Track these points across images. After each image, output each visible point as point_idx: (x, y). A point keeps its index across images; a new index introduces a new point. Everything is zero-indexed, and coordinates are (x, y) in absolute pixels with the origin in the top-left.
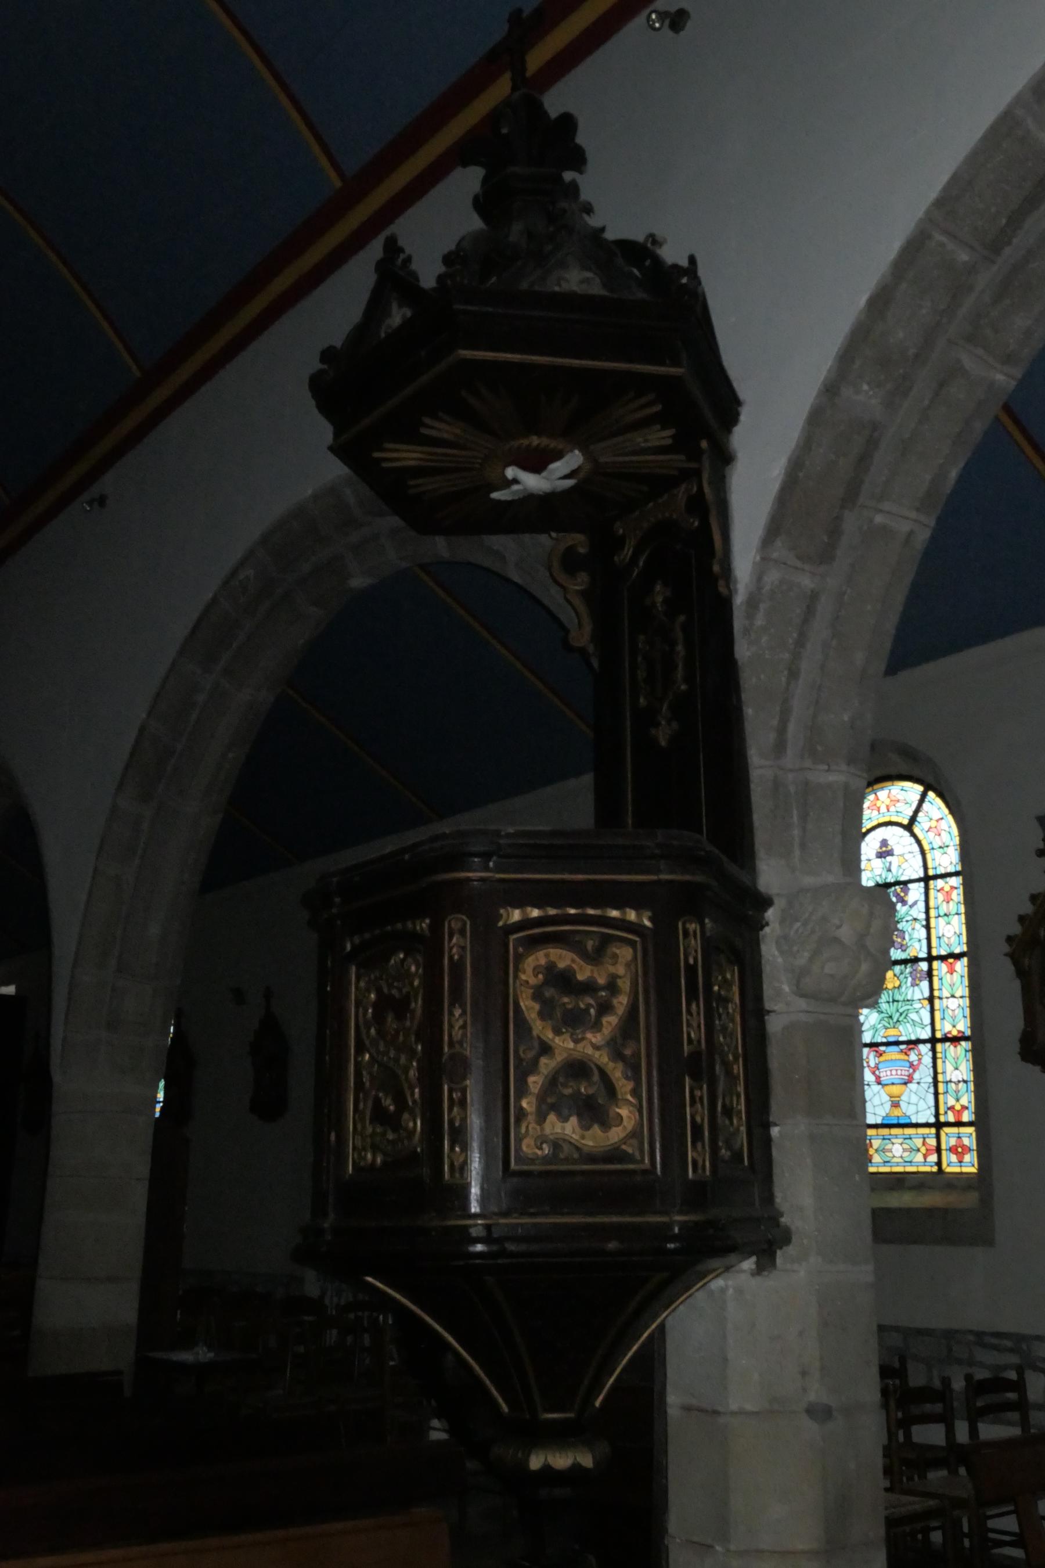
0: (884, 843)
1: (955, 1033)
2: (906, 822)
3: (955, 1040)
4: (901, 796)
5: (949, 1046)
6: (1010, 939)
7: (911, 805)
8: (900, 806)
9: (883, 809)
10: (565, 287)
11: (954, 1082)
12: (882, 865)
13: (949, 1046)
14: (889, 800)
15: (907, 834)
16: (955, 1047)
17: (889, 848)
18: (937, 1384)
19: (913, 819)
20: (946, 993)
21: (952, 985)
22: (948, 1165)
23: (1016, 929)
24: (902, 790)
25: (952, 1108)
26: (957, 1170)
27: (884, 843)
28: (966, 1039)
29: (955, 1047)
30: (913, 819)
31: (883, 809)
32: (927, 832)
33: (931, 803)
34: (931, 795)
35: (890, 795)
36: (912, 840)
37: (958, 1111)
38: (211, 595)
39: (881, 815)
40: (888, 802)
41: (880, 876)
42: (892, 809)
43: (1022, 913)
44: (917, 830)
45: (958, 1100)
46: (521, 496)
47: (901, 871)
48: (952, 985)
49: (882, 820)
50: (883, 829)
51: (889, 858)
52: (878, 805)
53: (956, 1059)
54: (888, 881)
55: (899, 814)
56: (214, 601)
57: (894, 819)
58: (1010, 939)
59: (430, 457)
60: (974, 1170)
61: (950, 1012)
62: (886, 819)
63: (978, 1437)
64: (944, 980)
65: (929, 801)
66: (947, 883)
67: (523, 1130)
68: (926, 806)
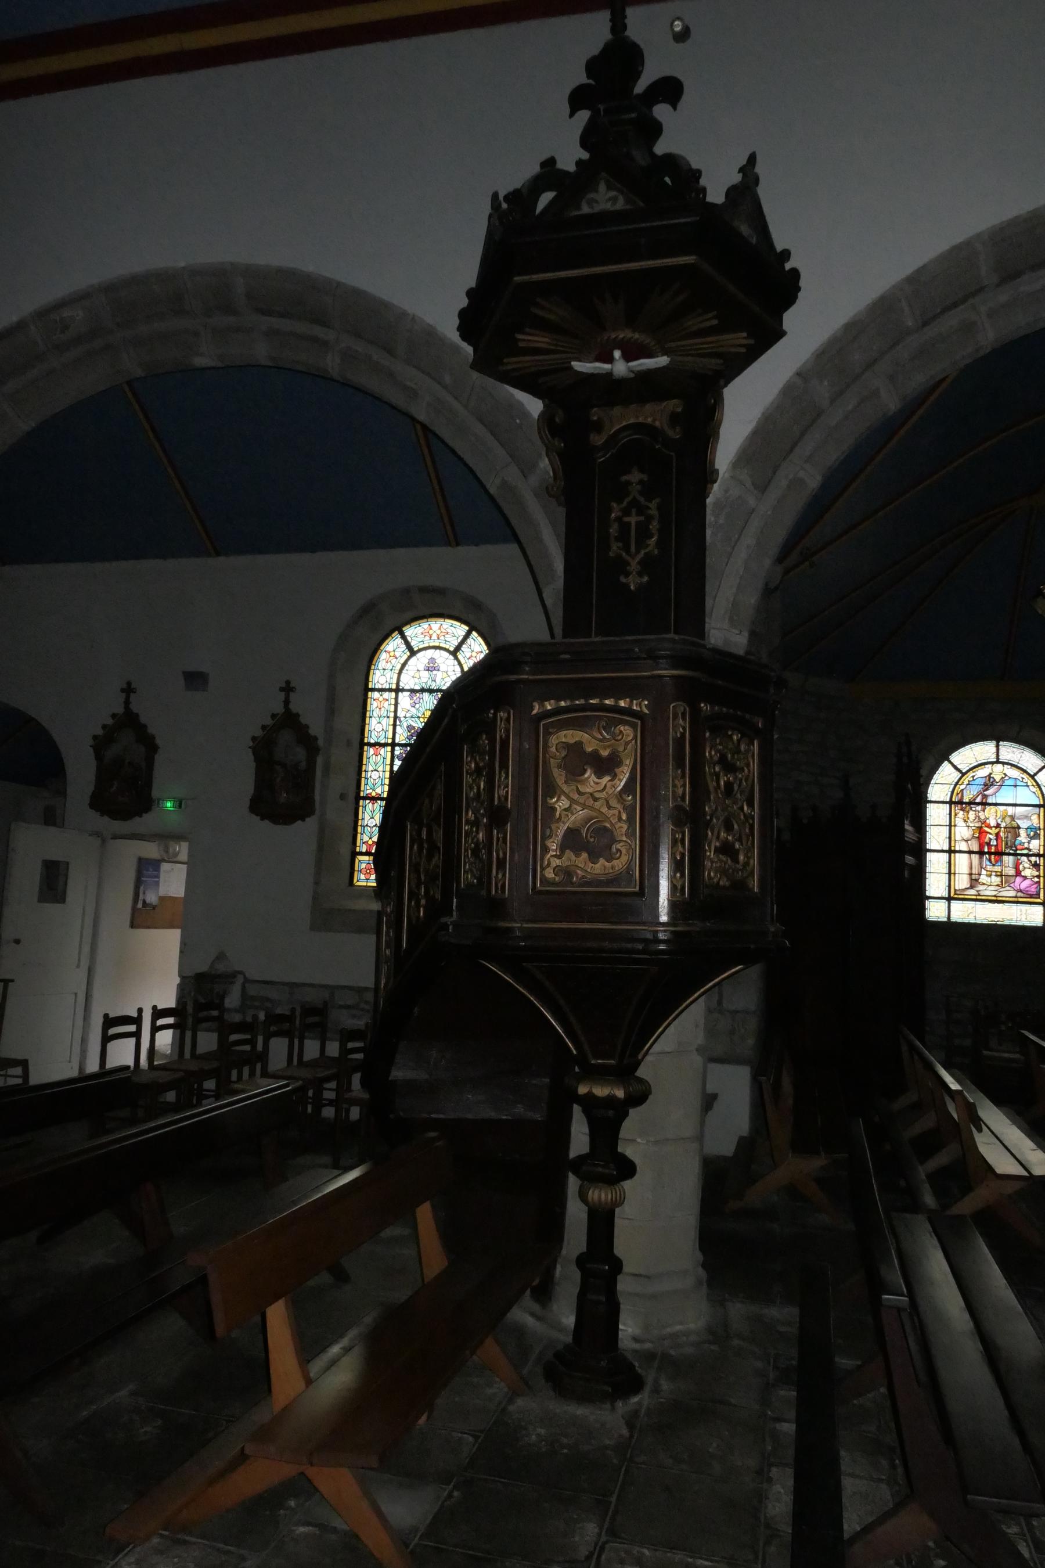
0: (432, 660)
1: (374, 794)
2: (452, 649)
3: (373, 799)
4: (451, 630)
5: (369, 803)
6: (254, 739)
7: (458, 638)
8: (448, 638)
9: (434, 637)
10: (598, 208)
11: (370, 827)
12: (428, 676)
13: (369, 803)
14: (439, 631)
15: (451, 657)
16: (373, 804)
17: (436, 665)
18: (249, 1019)
19: (458, 648)
20: (370, 768)
21: (376, 763)
22: (358, 881)
23: (100, 732)
24: (452, 626)
25: (366, 843)
26: (365, 884)
27: (432, 660)
28: (382, 799)
29: (373, 804)
30: (458, 648)
31: (434, 637)
32: (468, 659)
33: (474, 640)
34: (474, 634)
35: (441, 628)
36: (456, 663)
37: (370, 845)
38: (15, 319)
39: (431, 641)
40: (438, 632)
41: (426, 683)
42: (442, 638)
43: (105, 723)
44: (460, 656)
45: (371, 838)
46: (604, 372)
47: (443, 683)
48: (376, 763)
49: (432, 644)
50: (432, 651)
51: (435, 672)
52: (439, 631)
53: (373, 811)
54: (432, 687)
55: (447, 643)
56: (20, 326)
57: (442, 645)
58: (254, 739)
59: (701, 346)
60: (375, 884)
61: (372, 780)
62: (437, 644)
63: (28, 1082)
64: (371, 759)
65: (473, 638)
66: (381, 695)
67: (960, 795)
68: (469, 641)
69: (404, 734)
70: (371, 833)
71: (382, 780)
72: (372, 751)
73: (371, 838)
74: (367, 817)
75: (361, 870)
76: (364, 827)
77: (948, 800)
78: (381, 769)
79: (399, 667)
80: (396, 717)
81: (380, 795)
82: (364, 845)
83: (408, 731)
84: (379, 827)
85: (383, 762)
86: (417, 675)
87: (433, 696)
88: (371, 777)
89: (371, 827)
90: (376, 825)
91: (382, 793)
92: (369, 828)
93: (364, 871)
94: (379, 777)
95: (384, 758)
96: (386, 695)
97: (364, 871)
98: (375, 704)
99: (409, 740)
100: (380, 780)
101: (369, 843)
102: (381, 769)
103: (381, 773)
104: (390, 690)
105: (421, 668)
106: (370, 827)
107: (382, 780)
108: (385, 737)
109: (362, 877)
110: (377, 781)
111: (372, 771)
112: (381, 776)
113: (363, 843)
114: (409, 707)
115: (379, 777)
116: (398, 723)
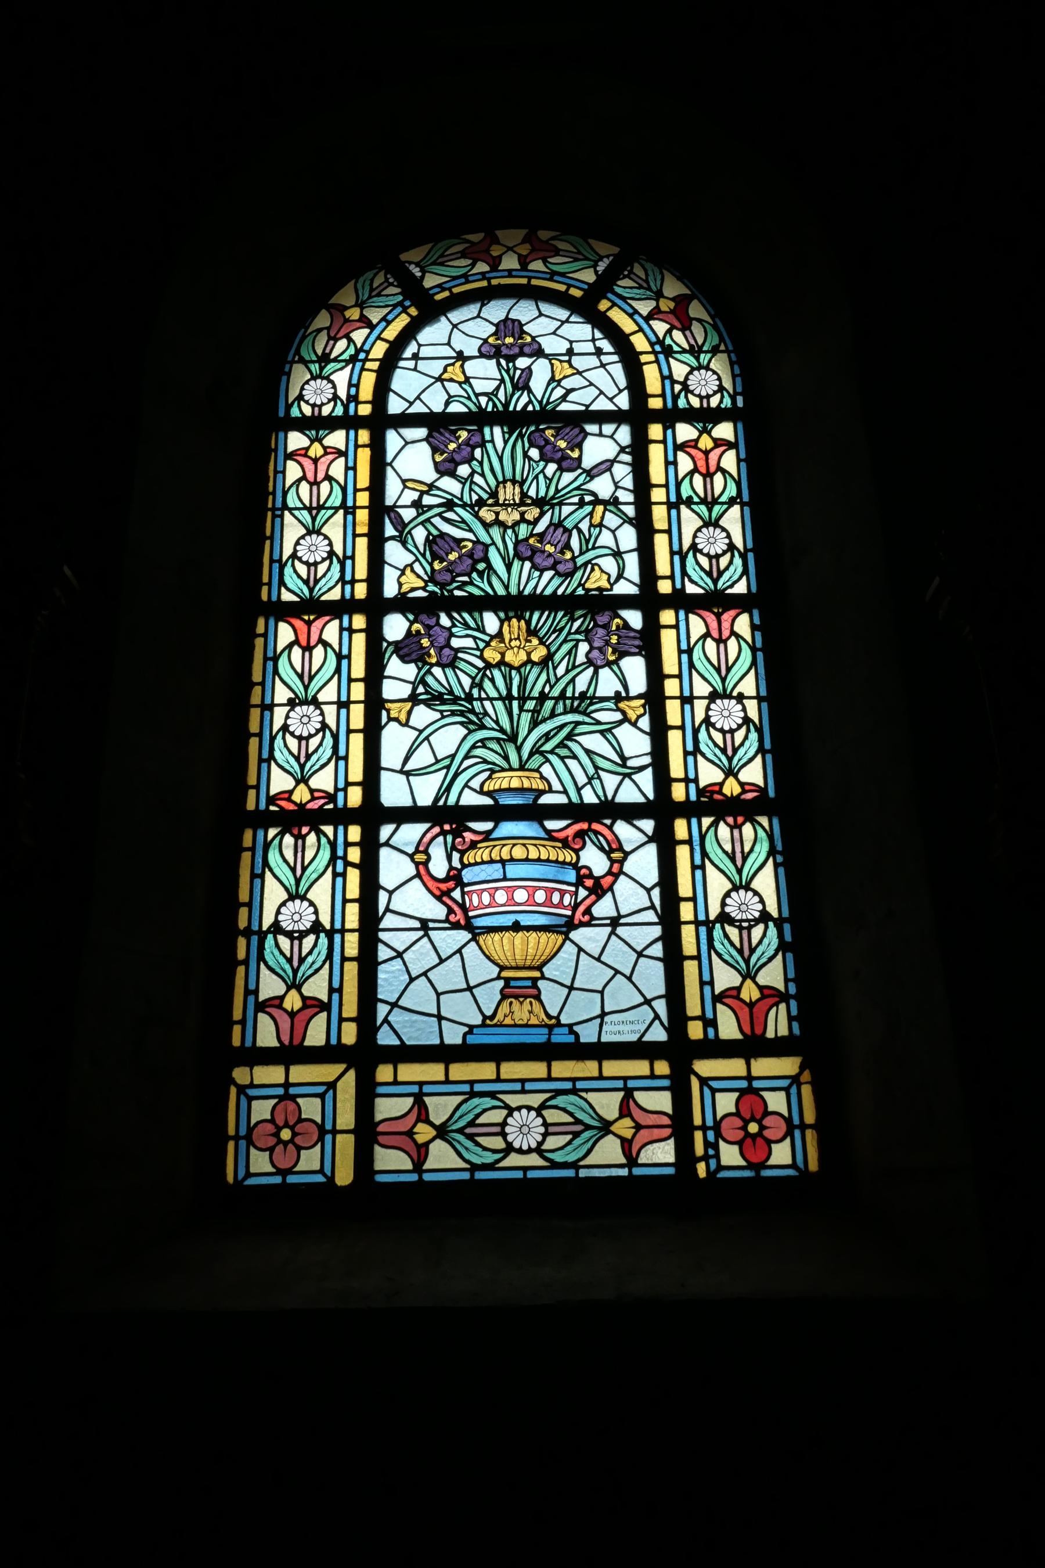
0: (509, 326)
20: (282, 694)
27: (509, 326)
45: (749, 975)
47: (559, 392)
48: (306, 677)
69: (417, 567)
70: (746, 951)
71: (335, 737)
72: (285, 633)
73: (295, 985)
74: (273, 894)
75: (250, 1130)
76: (262, 936)
77: (399, 959)
78: (329, 694)
79: (379, 350)
80: (379, 509)
81: (332, 798)
82: (262, 1017)
83: (435, 556)
84: (779, 923)
85: (338, 670)
86: (455, 372)
87: (521, 436)
88: (285, 728)
89: (745, 927)
90: (765, 917)
91: (337, 789)
92: (284, 942)
93: (775, 1128)
94: (324, 726)
95: (340, 657)
96: (337, 439)
97: (775, 1128)
98: (293, 471)
99: (442, 586)
100: (329, 741)
101: (745, 995)
102: (329, 694)
103: (330, 711)
104: (349, 422)
105: (471, 348)
106: (289, 935)
107: (335, 737)
108: (342, 579)
109: (310, 1160)
110: (314, 742)
111: (292, 703)
112: (331, 721)
113: (717, 999)
114: (429, 474)
115: (324, 726)
116: (390, 531)
